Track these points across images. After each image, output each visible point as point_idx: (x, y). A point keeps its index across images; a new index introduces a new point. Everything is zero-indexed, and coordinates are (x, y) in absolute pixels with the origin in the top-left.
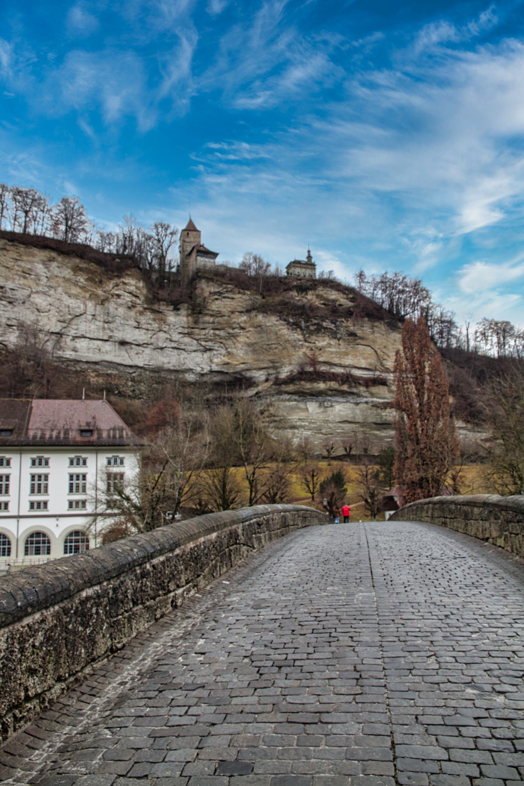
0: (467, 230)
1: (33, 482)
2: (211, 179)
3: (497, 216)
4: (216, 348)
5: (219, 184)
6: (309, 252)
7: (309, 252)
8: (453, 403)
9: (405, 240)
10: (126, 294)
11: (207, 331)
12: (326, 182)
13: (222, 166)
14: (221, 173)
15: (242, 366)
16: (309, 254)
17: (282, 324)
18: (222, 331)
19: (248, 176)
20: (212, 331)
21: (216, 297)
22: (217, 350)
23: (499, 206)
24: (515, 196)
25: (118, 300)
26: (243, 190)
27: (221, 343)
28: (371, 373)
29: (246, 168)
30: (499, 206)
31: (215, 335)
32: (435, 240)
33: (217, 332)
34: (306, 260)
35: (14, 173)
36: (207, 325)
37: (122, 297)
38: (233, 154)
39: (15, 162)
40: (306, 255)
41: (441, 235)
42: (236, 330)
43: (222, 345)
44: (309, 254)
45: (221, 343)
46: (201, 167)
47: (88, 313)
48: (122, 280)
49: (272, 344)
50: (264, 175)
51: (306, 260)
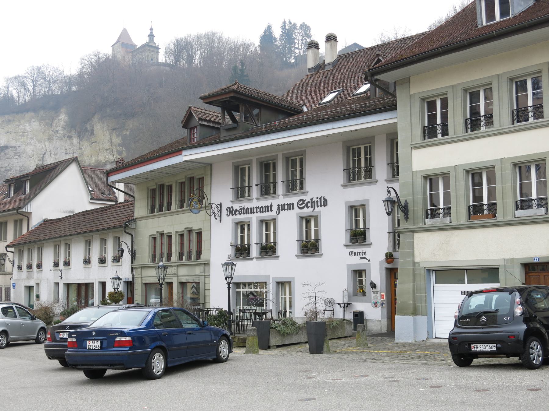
6: (151, 29)
7: (151, 29)
16: (151, 33)
44: (151, 33)
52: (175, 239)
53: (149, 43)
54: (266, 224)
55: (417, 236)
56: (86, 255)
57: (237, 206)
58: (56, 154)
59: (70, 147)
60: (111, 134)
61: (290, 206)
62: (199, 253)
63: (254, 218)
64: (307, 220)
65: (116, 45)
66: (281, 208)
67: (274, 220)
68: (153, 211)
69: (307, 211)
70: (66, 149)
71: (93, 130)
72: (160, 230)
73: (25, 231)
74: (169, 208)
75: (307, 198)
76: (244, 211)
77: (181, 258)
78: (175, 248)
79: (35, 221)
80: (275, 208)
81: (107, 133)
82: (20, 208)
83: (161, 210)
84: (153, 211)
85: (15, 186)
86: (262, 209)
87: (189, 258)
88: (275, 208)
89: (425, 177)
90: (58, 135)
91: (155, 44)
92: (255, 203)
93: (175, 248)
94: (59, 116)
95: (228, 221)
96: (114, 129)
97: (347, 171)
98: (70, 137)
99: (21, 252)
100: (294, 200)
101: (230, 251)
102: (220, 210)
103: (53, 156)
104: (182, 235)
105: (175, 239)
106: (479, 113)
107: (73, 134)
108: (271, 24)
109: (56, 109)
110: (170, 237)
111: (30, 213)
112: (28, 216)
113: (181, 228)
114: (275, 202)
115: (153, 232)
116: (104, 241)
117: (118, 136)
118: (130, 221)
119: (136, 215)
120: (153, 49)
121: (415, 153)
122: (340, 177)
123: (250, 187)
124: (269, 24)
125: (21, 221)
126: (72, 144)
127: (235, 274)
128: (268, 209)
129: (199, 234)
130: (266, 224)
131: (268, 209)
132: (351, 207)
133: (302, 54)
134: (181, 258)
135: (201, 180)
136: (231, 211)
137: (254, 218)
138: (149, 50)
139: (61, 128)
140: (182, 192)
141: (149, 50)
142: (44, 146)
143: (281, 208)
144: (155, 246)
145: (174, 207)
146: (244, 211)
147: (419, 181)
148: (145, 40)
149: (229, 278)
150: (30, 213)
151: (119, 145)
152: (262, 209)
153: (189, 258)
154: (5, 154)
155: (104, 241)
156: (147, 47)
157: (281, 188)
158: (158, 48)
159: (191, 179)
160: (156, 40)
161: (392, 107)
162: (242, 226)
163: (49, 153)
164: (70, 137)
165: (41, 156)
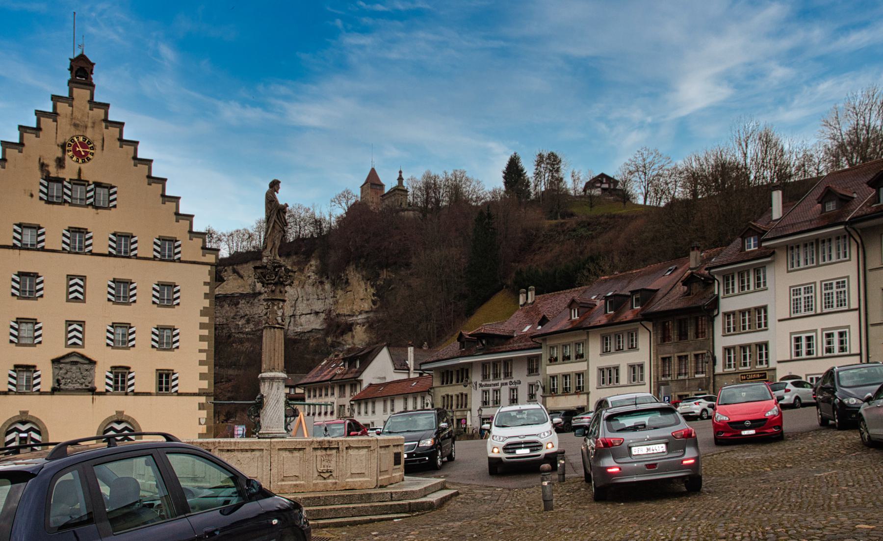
0: (684, 112)
1: (798, 350)
2: (352, 40)
3: (724, 92)
5: (362, 47)
6: (400, 172)
7: (400, 172)
8: (240, 424)
9: (602, 127)
12: (502, 43)
13: (366, 21)
14: (365, 30)
16: (400, 176)
19: (401, 35)
23: (726, 78)
24: (750, 64)
26: (394, 55)
28: (841, 246)
29: (398, 24)
30: (726, 78)
32: (641, 126)
35: (92, 30)
38: (381, 3)
39: (94, 14)
41: (649, 119)
44: (400, 176)
46: (339, 23)
50: (421, 34)
52: (454, 398)
53: (398, 186)
54: (496, 391)
55: (547, 398)
56: (413, 405)
57: (483, 383)
58: (308, 300)
59: (322, 292)
60: (366, 283)
61: (506, 384)
62: (466, 405)
63: (491, 389)
64: (513, 390)
65: (365, 186)
66: (502, 384)
67: (499, 390)
68: (443, 384)
69: (513, 386)
70: (318, 295)
71: (348, 279)
72: (447, 393)
73: (358, 391)
74: (451, 383)
75: (513, 381)
76: (486, 385)
77: (457, 407)
78: (454, 402)
79: (365, 385)
80: (500, 384)
81: (362, 283)
82: (358, 377)
83: (447, 383)
84: (443, 384)
85: (348, 362)
86: (494, 385)
87: (461, 407)
88: (500, 384)
89: (551, 377)
90: (310, 281)
91: (404, 187)
92: (491, 382)
93: (454, 402)
94: (309, 261)
95: (480, 389)
96: (368, 280)
97: (529, 369)
98: (322, 283)
99: (359, 405)
100: (508, 381)
101: (480, 405)
102: (476, 385)
103: (305, 302)
104: (458, 396)
105: (454, 398)
106: (389, 478)
107: (324, 279)
108: (519, 154)
109: (308, 256)
110: (452, 397)
111: (362, 380)
112: (360, 382)
113: (457, 393)
114: (500, 382)
115: (443, 394)
116: (415, 399)
117: (372, 286)
118: (431, 388)
119: (434, 385)
120: (403, 193)
121: (548, 367)
122: (526, 372)
123: (489, 375)
124: (515, 154)
125: (356, 385)
126: (323, 290)
127: (483, 414)
128: (497, 385)
129: (466, 395)
130: (496, 391)
131: (497, 385)
132: (530, 385)
133: (548, 188)
134: (457, 407)
135: (467, 371)
136: (481, 385)
137: (491, 389)
138: (398, 194)
139: (313, 274)
140: (458, 375)
141: (398, 194)
142: (296, 292)
143: (502, 384)
144: (444, 401)
145: (454, 382)
146: (486, 385)
147: (549, 378)
148: (395, 183)
149: (480, 415)
150: (362, 380)
151: (374, 295)
152: (494, 385)
153: (461, 407)
154: (259, 300)
155: (415, 399)
156: (397, 192)
157: (502, 376)
158: (406, 191)
159: (463, 369)
160: (405, 184)
161: (541, 347)
162: (485, 392)
163: (301, 299)
164: (322, 283)
165: (294, 302)
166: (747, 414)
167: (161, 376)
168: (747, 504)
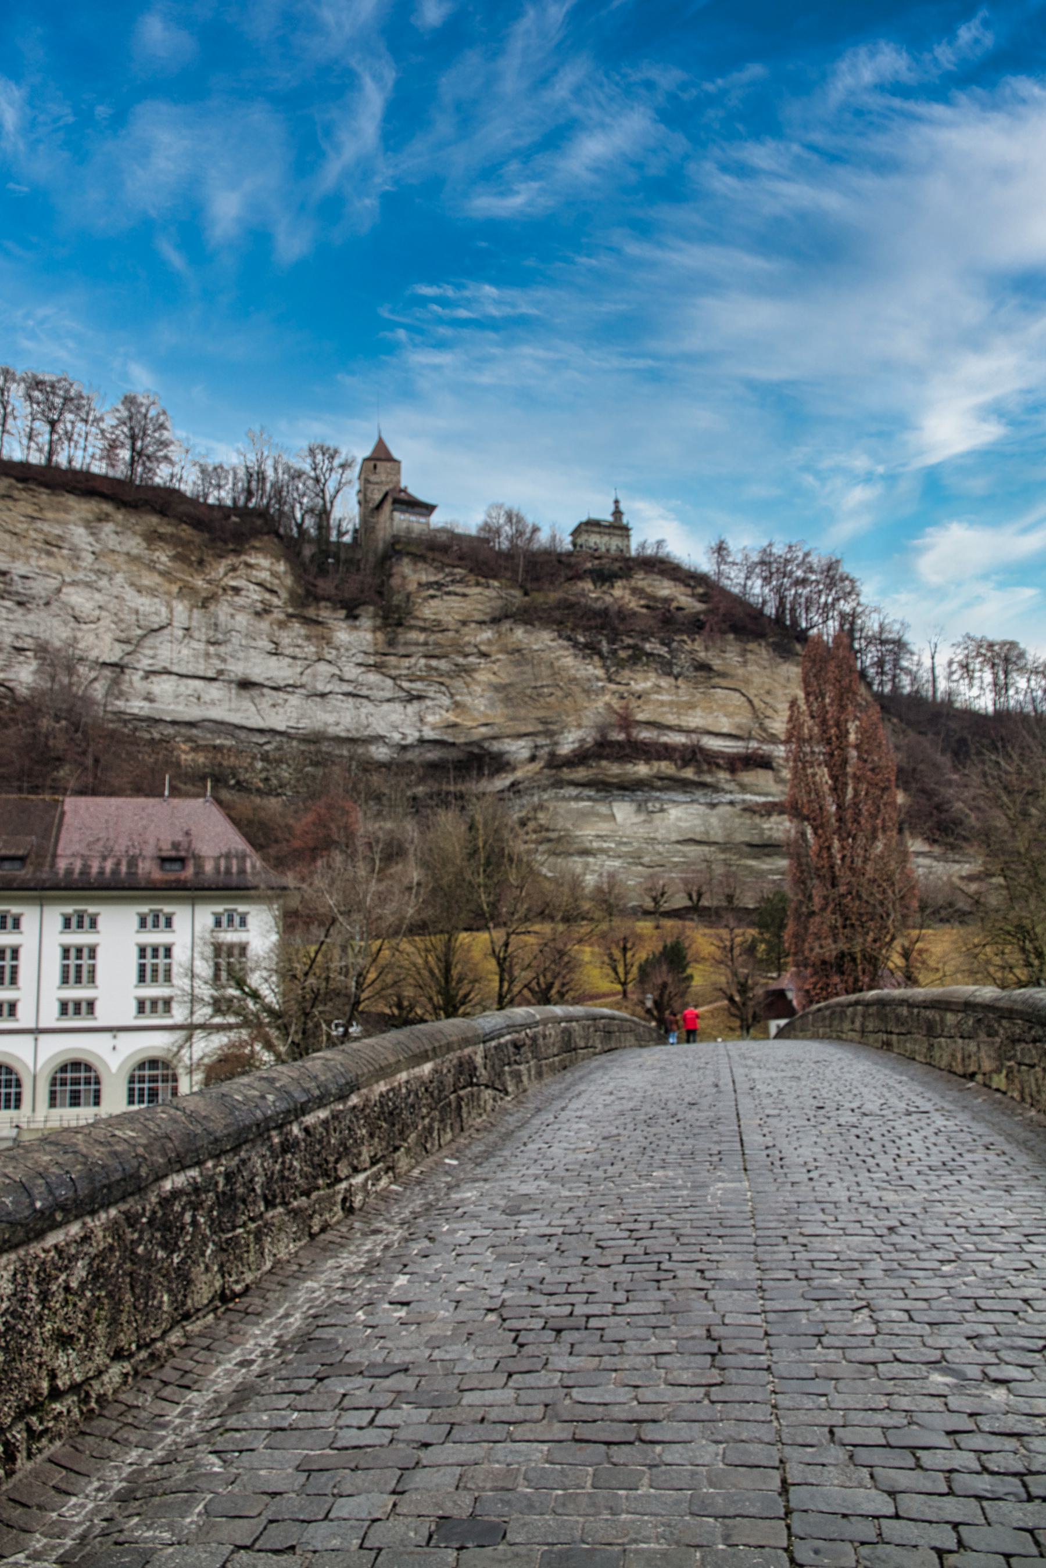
0: (932, 459)
2: (421, 358)
3: (991, 432)
4: (431, 694)
5: (437, 368)
6: (616, 502)
7: (616, 502)
9: (809, 480)
10: (252, 587)
11: (413, 660)
12: (650, 362)
13: (443, 331)
14: (441, 345)
15: (483, 730)
16: (617, 507)
17: (562, 647)
18: (443, 661)
19: (496, 351)
20: (423, 661)
21: (431, 592)
22: (433, 699)
23: (996, 411)
24: (1029, 391)
25: (236, 599)
26: (485, 379)
27: (442, 684)
29: (491, 335)
30: (996, 411)
31: (430, 668)
32: (868, 478)
33: (434, 663)
34: (610, 519)
35: (27, 344)
36: (413, 649)
37: (243, 593)
38: (465, 308)
39: (30, 323)
40: (612, 508)
41: (881, 469)
42: (471, 659)
43: (443, 689)
44: (617, 507)
45: (442, 684)
46: (401, 334)
47: (175, 624)
48: (244, 558)
49: (542, 686)
50: (527, 350)
51: (610, 519)
166: (674, 801)
167: (93, 982)
168: (666, 875)
